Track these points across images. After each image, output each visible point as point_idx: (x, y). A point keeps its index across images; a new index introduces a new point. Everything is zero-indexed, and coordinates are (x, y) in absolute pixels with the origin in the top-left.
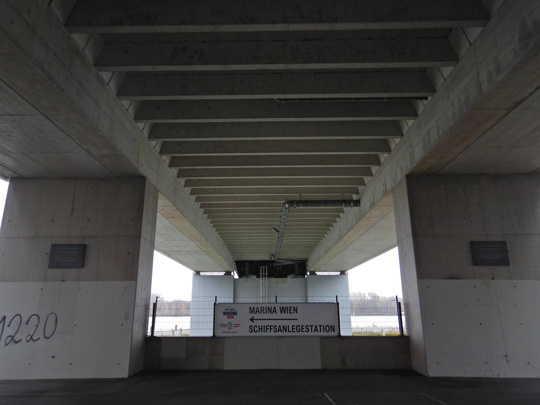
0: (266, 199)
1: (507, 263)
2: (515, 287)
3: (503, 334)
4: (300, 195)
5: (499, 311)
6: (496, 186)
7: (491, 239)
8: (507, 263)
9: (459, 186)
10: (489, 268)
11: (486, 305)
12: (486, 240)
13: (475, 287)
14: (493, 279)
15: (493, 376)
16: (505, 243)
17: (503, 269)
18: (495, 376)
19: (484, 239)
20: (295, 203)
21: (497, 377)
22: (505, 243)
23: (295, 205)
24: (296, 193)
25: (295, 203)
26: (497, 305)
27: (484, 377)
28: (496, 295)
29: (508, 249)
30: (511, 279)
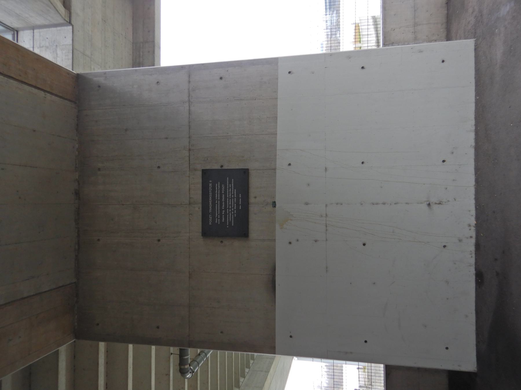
0: (182, 388)
1: (246, 172)
2: (290, 164)
3: (384, 204)
4: (172, 354)
5: (337, 204)
6: (99, 169)
7: (198, 196)
8: (246, 172)
9: (99, 240)
10: (253, 209)
11: (327, 268)
12: (200, 205)
13: (290, 243)
14: (274, 204)
15: (471, 237)
16: (205, 173)
17: (254, 182)
18: (473, 233)
19: (198, 210)
20: (182, 367)
21: (473, 229)
22: (205, 173)
23: (186, 367)
24: (169, 361)
25: (182, 367)
26: (326, 206)
27: (474, 255)
28: (307, 204)
29: (217, 167)
30: (275, 169)
